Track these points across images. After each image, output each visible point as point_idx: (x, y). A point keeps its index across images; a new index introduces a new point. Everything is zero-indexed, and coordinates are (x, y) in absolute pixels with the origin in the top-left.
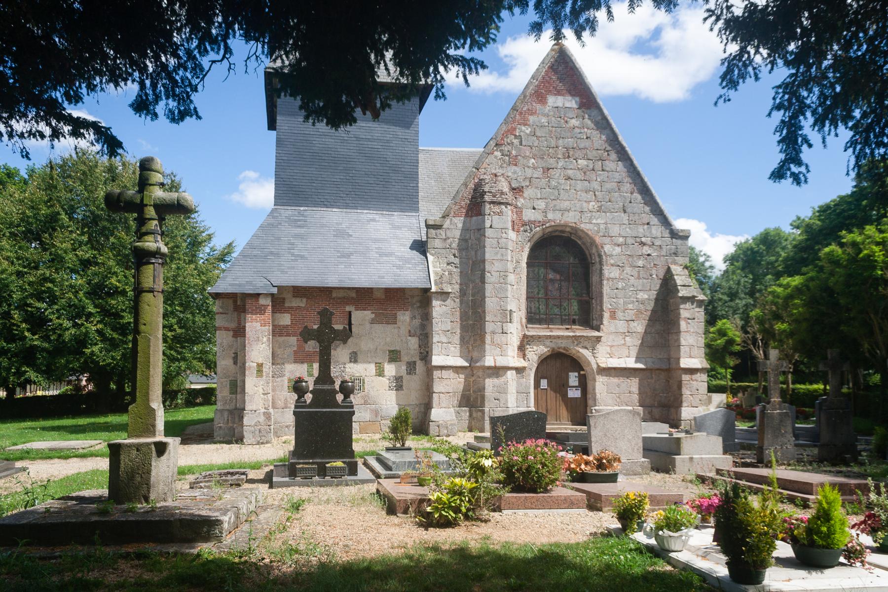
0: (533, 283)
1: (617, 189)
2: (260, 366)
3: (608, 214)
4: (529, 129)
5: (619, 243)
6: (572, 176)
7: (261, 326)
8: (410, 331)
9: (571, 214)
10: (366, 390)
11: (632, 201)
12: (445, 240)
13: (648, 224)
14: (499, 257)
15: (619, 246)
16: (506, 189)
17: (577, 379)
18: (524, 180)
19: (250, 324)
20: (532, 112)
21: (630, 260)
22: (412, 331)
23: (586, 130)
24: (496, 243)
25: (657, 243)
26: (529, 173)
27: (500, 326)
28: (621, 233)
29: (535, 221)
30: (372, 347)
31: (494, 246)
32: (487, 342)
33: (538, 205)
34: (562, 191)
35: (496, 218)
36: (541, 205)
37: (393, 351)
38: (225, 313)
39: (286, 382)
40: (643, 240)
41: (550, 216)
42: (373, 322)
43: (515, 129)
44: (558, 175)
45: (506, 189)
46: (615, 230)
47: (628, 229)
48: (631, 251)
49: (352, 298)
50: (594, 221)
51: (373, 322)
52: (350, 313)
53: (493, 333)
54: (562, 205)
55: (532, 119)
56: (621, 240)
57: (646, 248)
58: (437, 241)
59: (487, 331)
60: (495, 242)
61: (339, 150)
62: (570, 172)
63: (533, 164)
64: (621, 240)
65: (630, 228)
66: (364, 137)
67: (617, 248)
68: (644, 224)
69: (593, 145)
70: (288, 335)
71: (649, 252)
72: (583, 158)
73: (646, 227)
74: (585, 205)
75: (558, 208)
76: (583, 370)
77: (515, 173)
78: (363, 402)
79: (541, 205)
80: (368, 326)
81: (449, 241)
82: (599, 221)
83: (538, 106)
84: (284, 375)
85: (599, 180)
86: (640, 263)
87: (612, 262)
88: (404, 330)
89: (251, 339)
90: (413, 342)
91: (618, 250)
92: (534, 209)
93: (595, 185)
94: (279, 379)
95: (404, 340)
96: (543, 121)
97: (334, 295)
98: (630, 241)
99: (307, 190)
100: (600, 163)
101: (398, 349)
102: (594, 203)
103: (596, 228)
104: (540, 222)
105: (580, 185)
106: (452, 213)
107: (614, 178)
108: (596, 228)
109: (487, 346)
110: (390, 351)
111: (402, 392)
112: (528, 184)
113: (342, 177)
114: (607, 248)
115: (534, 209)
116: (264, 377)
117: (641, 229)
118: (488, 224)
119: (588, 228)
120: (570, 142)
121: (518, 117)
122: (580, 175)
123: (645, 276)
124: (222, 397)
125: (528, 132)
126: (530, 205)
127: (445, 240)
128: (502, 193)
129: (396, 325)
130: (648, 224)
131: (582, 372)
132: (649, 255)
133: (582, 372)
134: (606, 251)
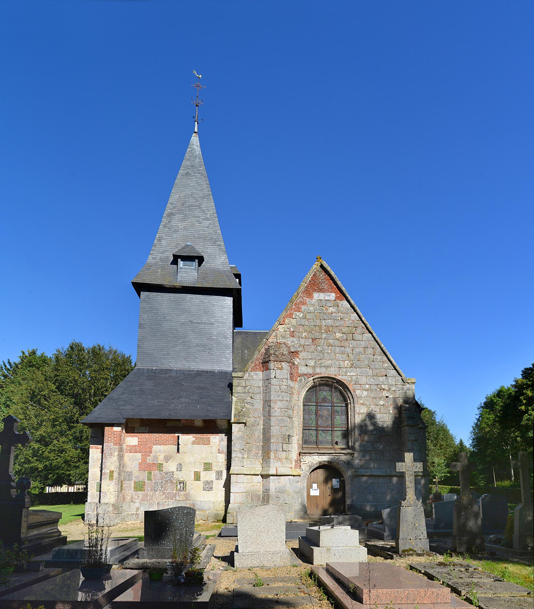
0: (307, 416)
1: (363, 352)
2: (112, 472)
3: (358, 369)
4: (302, 314)
5: (366, 388)
6: (332, 344)
7: (114, 445)
8: (219, 450)
9: (332, 369)
10: (187, 491)
11: (374, 360)
12: (245, 387)
13: (386, 376)
14: (280, 398)
15: (366, 390)
16: (286, 352)
17: (338, 483)
18: (299, 347)
19: (106, 444)
20: (304, 304)
21: (374, 400)
22: (221, 450)
23: (340, 314)
24: (278, 388)
25: (394, 389)
26: (302, 341)
27: (281, 446)
28: (367, 382)
29: (307, 374)
30: (192, 461)
31: (277, 391)
32: (271, 457)
33: (309, 363)
34: (326, 354)
35: (278, 371)
36: (312, 363)
37: (207, 463)
38: (96, 437)
39: (133, 484)
40: (383, 386)
41: (318, 370)
42: (194, 443)
43: (292, 314)
44: (322, 343)
45: (286, 352)
46: (363, 380)
47: (372, 379)
48: (374, 395)
49: (467, 455)
50: (348, 374)
51: (194, 443)
52: (178, 436)
53: (276, 450)
54: (326, 363)
55: (303, 307)
56: (367, 386)
57: (385, 392)
58: (239, 388)
59: (271, 449)
60: (278, 387)
61: (179, 330)
62: (331, 341)
63: (305, 335)
64: (367, 386)
65: (373, 379)
66: (196, 321)
67: (364, 392)
68: (383, 376)
69: (345, 324)
70: (136, 452)
71: (387, 395)
72: (339, 332)
73: (384, 377)
74: (342, 363)
75: (323, 365)
76: (343, 477)
77: (293, 342)
78: (185, 499)
79: (312, 363)
80: (190, 446)
81: (248, 388)
82: (352, 374)
83: (308, 300)
84: (132, 480)
85: (351, 346)
86: (381, 403)
87: (362, 402)
88: (215, 450)
89: (107, 454)
90: (221, 457)
91: (365, 393)
92: (307, 366)
93: (349, 350)
94: (128, 482)
95: (215, 456)
96: (311, 309)
97: (168, 425)
98: (374, 387)
99: (158, 356)
100: (351, 335)
101: (211, 462)
102: (348, 362)
103: (350, 379)
104: (311, 374)
105: (338, 349)
106: (250, 369)
107: (361, 345)
108: (350, 379)
109: (272, 460)
110: (204, 464)
111: (212, 492)
112: (301, 349)
113: (181, 347)
114: (358, 392)
115: (307, 366)
116: (114, 480)
117: (381, 379)
118: (273, 376)
119: (344, 378)
120: (330, 322)
121: (294, 306)
122: (337, 343)
123: (385, 411)
124: (91, 493)
125: (301, 316)
126: (304, 363)
127: (245, 387)
128: (283, 355)
129: (209, 446)
130: (386, 376)
131: (342, 479)
132: (387, 397)
133: (342, 479)
134: (357, 395)
